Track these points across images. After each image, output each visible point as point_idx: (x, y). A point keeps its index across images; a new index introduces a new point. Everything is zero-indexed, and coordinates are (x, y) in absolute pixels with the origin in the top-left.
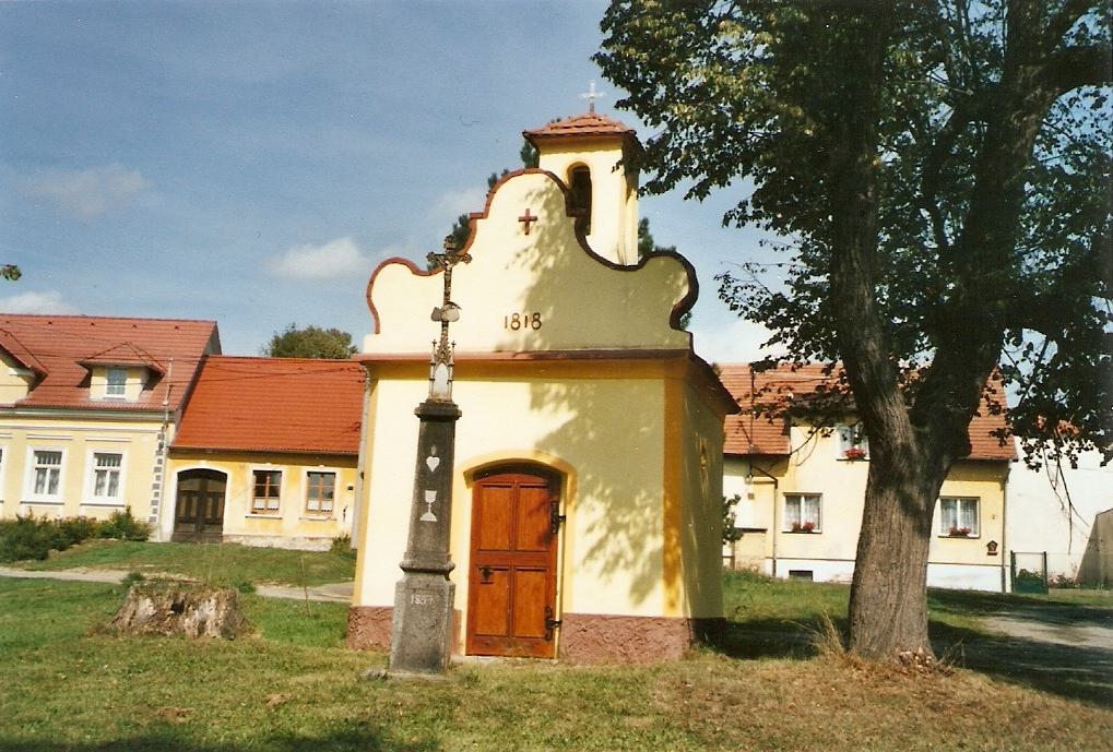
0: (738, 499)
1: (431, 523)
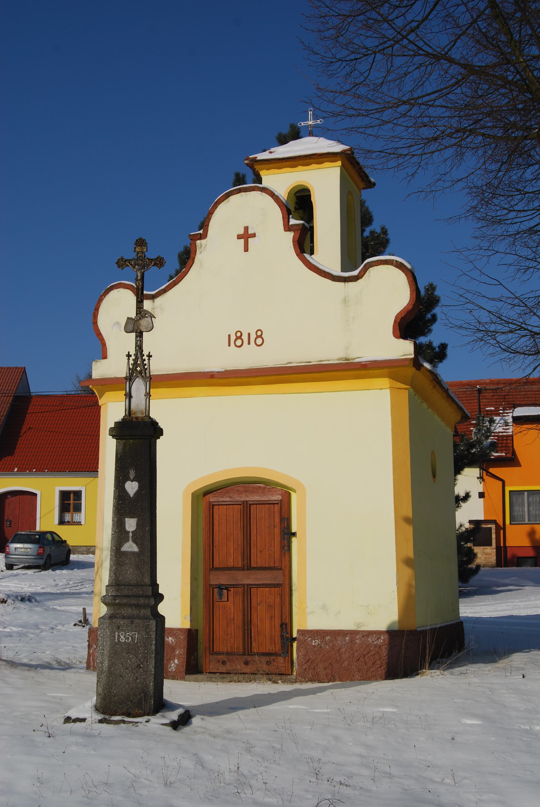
0: (467, 497)
1: (133, 553)
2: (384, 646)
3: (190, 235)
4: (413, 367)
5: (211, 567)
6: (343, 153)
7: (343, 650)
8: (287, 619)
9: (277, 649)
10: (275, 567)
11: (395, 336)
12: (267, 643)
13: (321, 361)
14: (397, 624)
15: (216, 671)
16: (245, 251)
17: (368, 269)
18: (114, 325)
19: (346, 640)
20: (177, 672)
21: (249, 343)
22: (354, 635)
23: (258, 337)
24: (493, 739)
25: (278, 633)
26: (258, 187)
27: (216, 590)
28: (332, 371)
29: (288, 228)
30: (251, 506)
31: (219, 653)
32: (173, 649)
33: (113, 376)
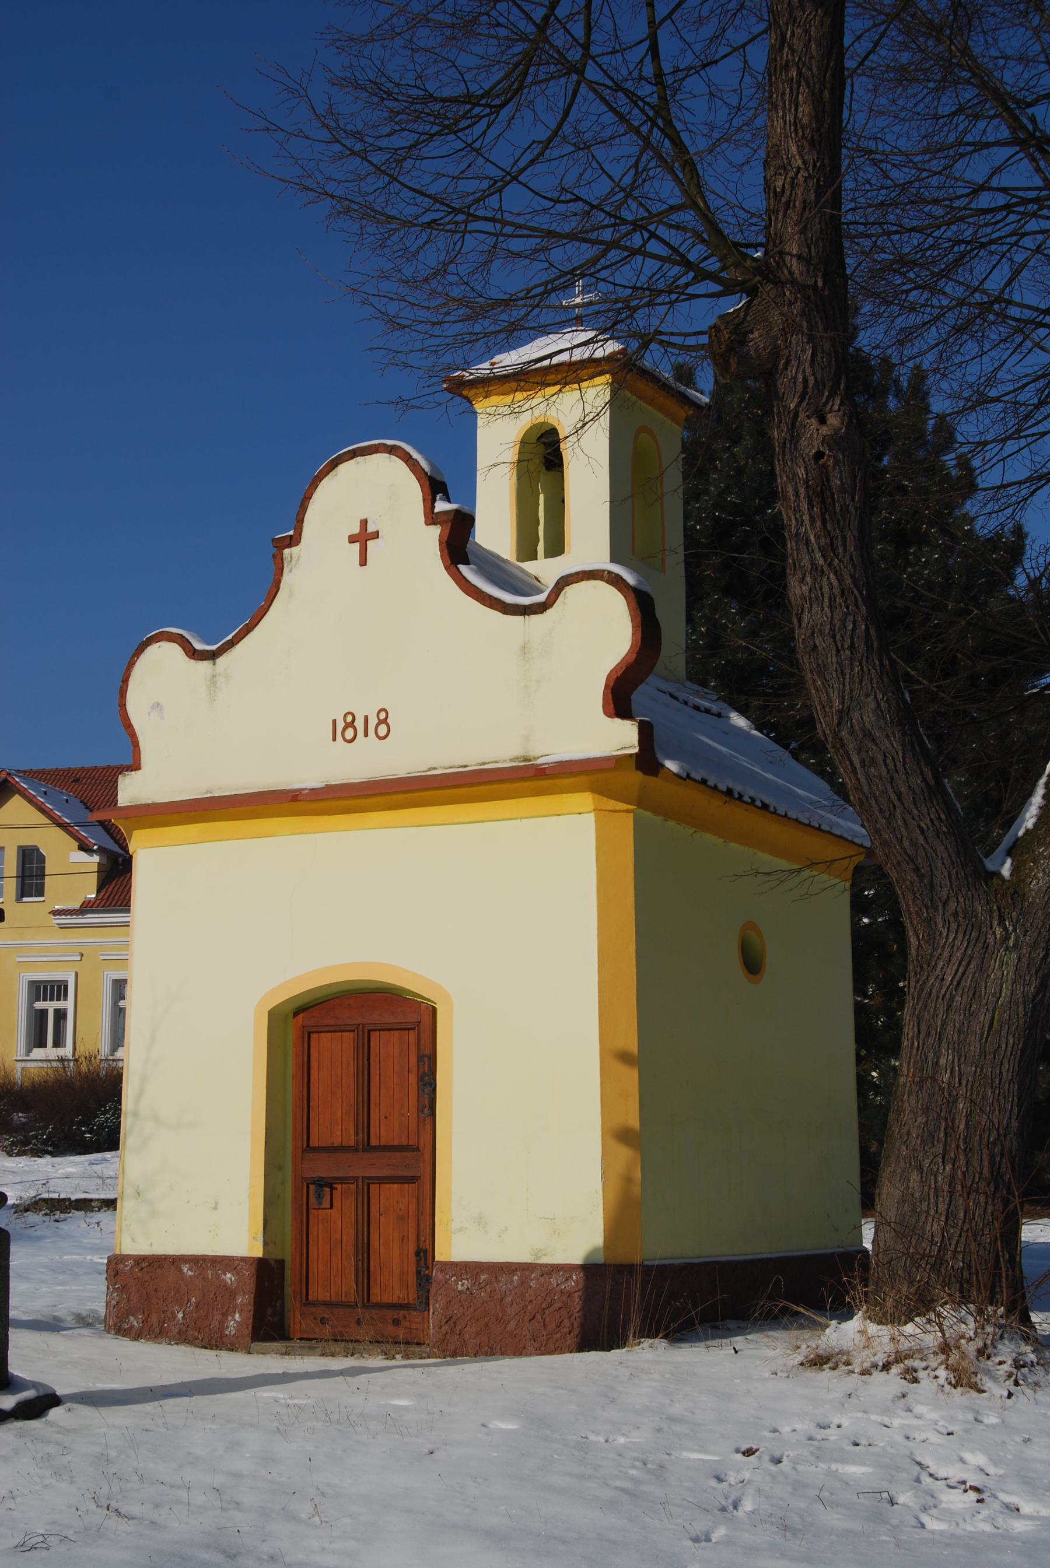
2: (577, 1294)
3: (274, 540)
4: (637, 769)
5: (305, 1146)
6: (610, 358)
7: (509, 1299)
8: (427, 1241)
9: (411, 1298)
10: (408, 1145)
11: (607, 713)
12: (395, 1287)
13: (484, 764)
14: (602, 1252)
15: (311, 1336)
16: (361, 565)
17: (563, 589)
18: (153, 708)
19: (512, 1281)
20: (237, 1338)
21: (366, 735)
22: (527, 1273)
23: (380, 722)
24: (495, 1454)
25: (413, 1269)
26: (384, 445)
27: (312, 1187)
28: (501, 781)
29: (431, 518)
30: (371, 1033)
31: (316, 1304)
32: (233, 1294)
33: (149, 802)
